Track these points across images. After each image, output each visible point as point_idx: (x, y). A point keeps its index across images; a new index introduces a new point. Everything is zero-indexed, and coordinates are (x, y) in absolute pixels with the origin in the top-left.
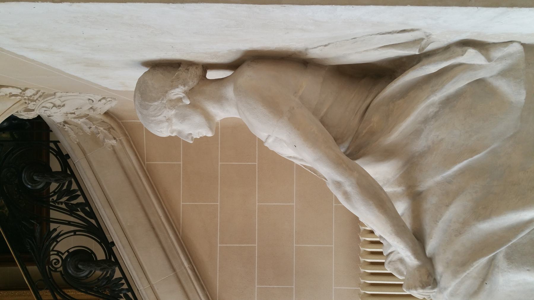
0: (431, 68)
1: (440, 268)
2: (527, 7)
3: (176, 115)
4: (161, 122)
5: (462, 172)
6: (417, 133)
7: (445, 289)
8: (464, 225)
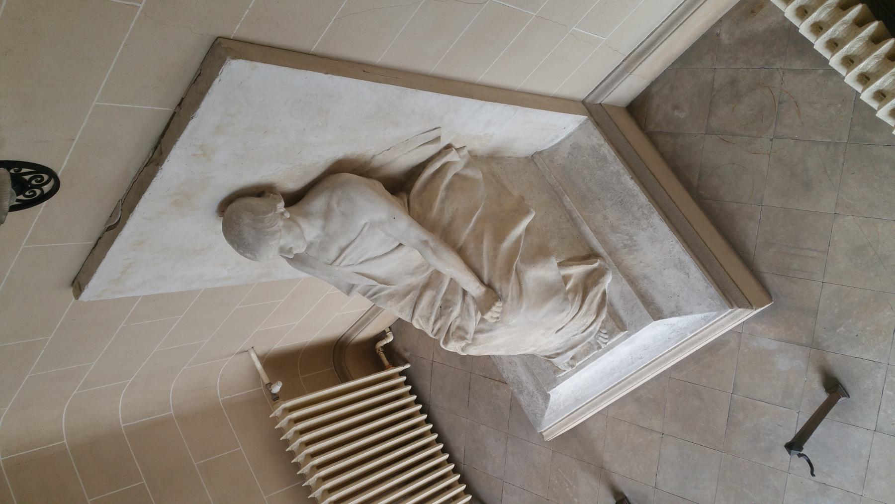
0: (437, 165)
1: (497, 285)
2: (481, 99)
3: (284, 226)
4: (276, 232)
5: (477, 221)
6: (442, 210)
7: (507, 296)
8: (495, 249)
